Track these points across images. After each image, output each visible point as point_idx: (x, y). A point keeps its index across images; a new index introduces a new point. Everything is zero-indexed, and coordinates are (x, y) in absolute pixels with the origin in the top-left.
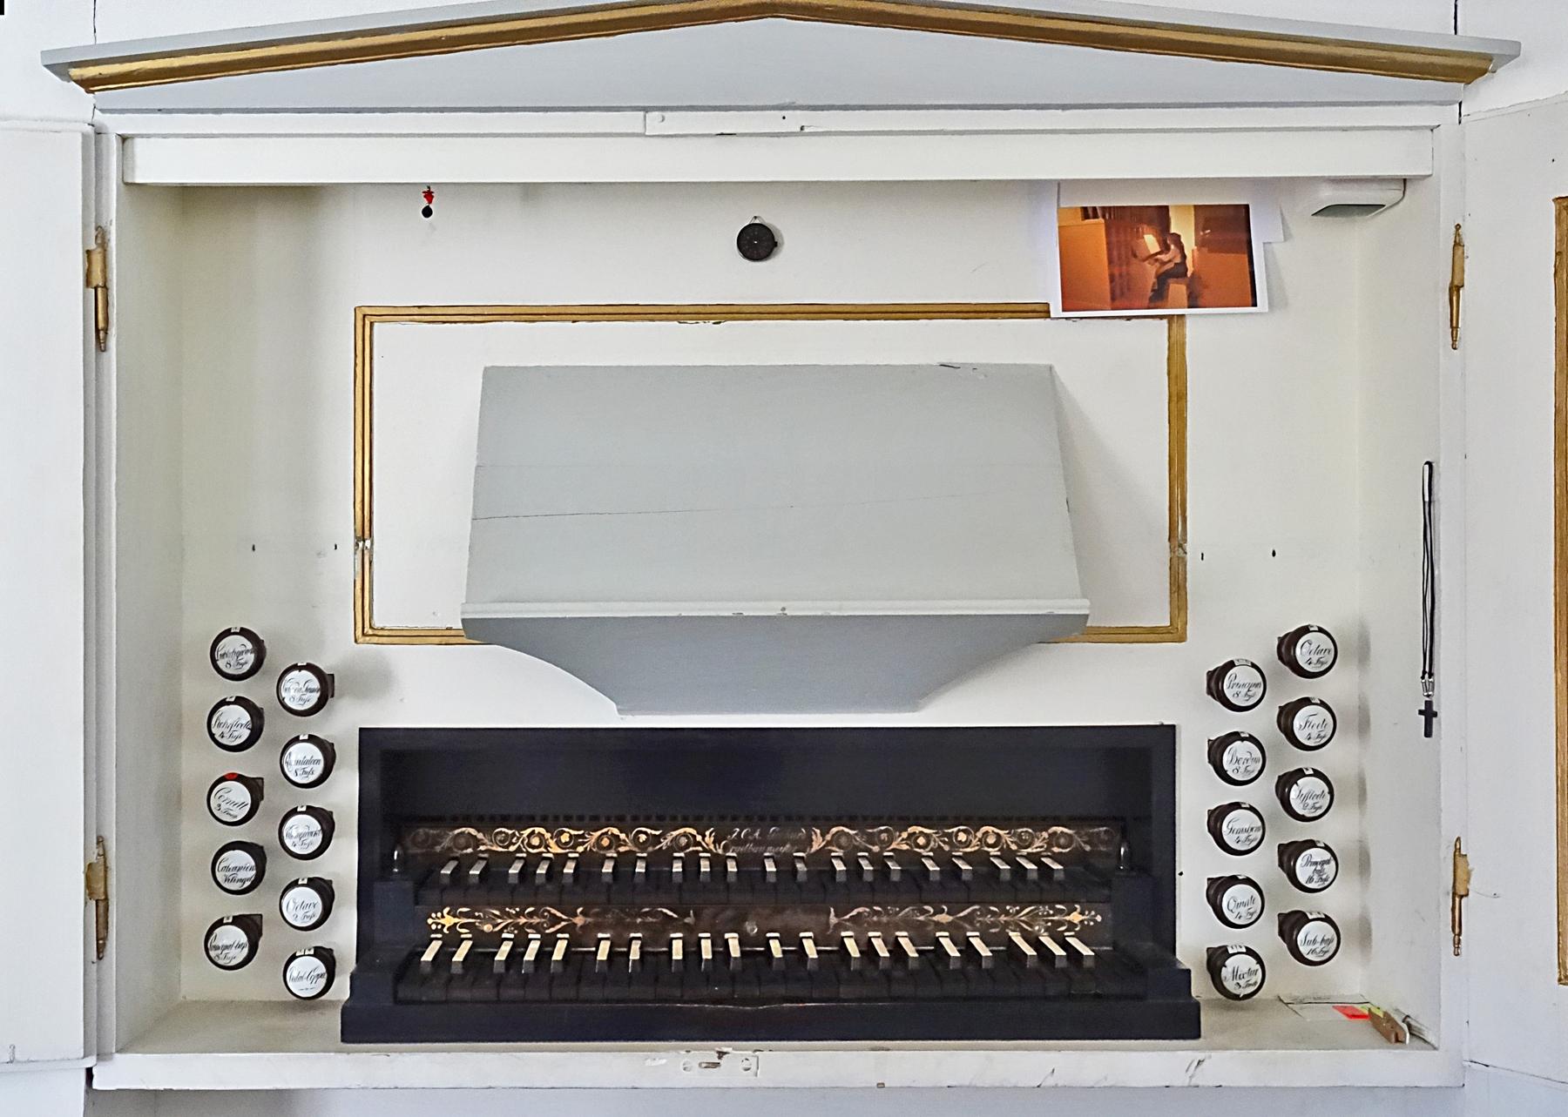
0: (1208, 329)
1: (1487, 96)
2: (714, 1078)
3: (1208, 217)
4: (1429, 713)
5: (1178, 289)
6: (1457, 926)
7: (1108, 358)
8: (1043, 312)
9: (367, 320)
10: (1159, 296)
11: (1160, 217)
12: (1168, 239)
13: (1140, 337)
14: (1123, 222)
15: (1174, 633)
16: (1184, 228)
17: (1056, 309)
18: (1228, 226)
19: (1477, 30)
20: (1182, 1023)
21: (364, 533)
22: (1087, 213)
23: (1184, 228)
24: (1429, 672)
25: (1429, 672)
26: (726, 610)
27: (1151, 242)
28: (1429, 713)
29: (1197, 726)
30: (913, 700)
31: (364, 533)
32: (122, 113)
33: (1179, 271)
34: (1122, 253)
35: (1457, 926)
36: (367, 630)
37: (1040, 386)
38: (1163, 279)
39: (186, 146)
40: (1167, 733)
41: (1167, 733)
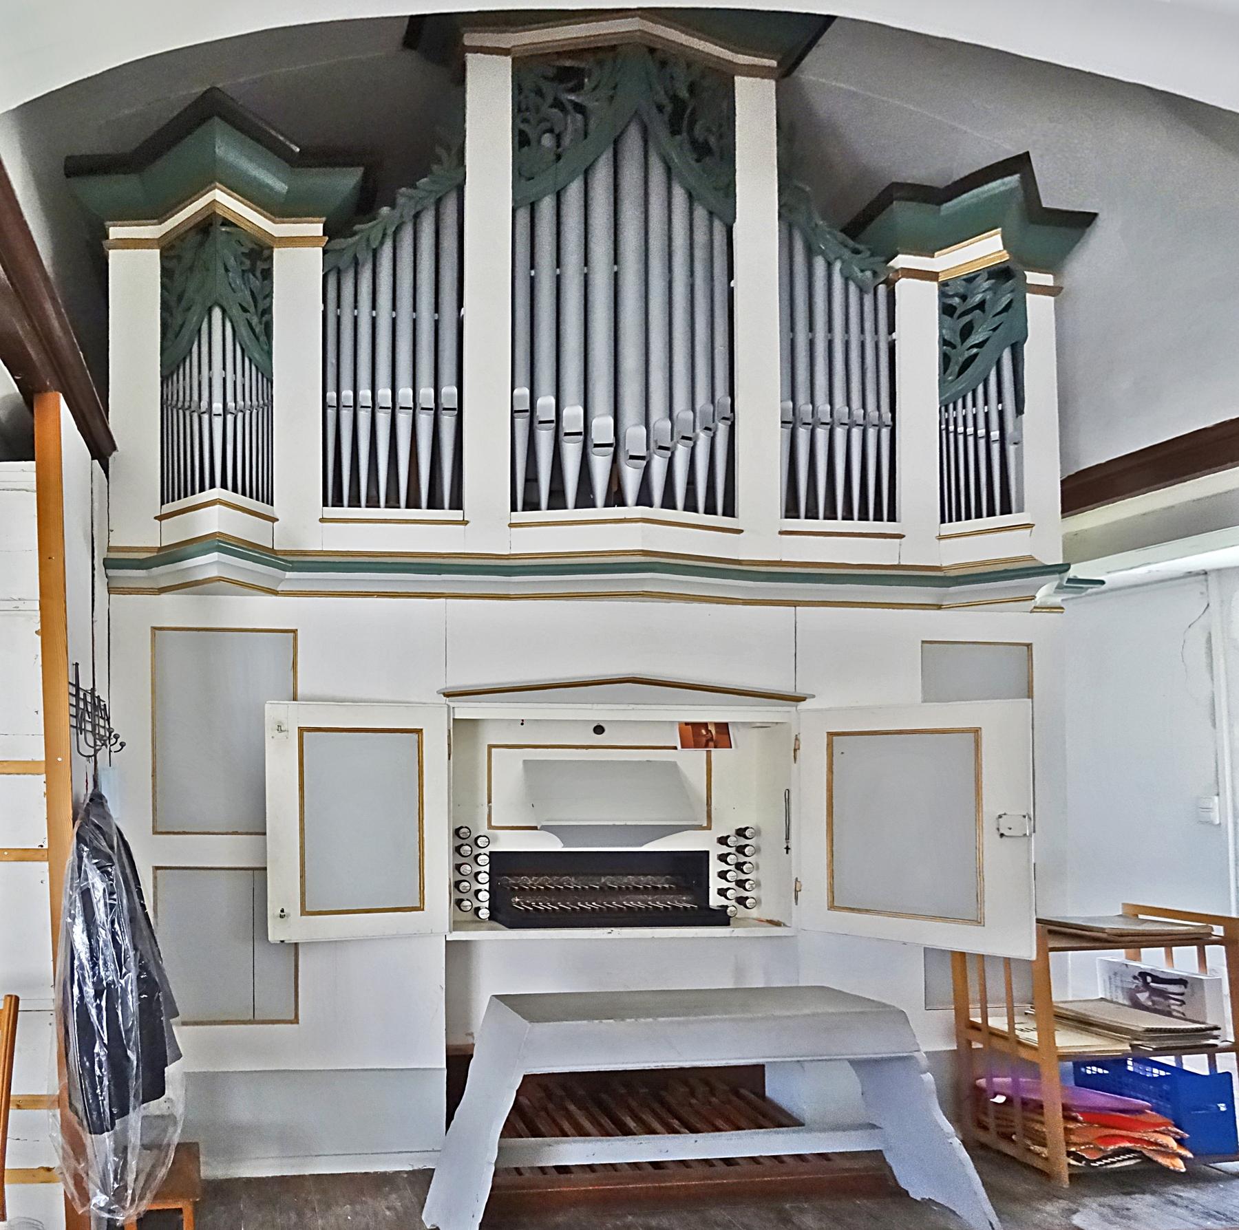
0: (715, 752)
1: (802, 705)
2: (610, 936)
3: (717, 725)
4: (787, 848)
5: (711, 744)
6: (796, 898)
7: (692, 761)
8: (675, 748)
9: (490, 747)
10: (706, 746)
11: (705, 725)
12: (708, 731)
13: (701, 753)
14: (696, 726)
15: (709, 828)
16: (712, 729)
17: (679, 747)
18: (723, 727)
19: (801, 691)
20: (728, 924)
21: (489, 802)
22: (687, 724)
23: (712, 729)
24: (787, 838)
25: (787, 838)
26: (611, 823)
27: (704, 732)
28: (787, 848)
29: (715, 850)
30: (641, 845)
31: (489, 802)
32: (453, 702)
33: (712, 739)
34: (696, 734)
35: (796, 898)
36: (490, 827)
37: (674, 765)
38: (707, 741)
39: (466, 710)
40: (707, 853)
41: (707, 853)
